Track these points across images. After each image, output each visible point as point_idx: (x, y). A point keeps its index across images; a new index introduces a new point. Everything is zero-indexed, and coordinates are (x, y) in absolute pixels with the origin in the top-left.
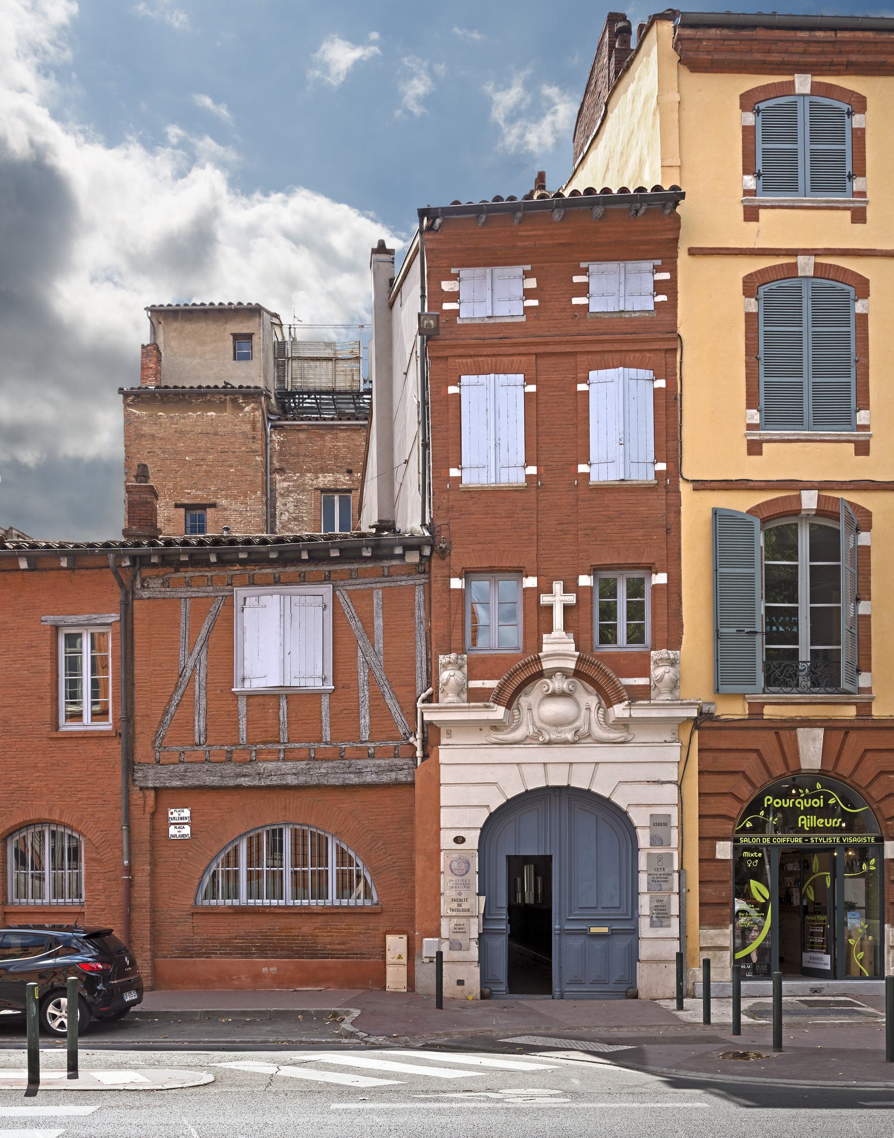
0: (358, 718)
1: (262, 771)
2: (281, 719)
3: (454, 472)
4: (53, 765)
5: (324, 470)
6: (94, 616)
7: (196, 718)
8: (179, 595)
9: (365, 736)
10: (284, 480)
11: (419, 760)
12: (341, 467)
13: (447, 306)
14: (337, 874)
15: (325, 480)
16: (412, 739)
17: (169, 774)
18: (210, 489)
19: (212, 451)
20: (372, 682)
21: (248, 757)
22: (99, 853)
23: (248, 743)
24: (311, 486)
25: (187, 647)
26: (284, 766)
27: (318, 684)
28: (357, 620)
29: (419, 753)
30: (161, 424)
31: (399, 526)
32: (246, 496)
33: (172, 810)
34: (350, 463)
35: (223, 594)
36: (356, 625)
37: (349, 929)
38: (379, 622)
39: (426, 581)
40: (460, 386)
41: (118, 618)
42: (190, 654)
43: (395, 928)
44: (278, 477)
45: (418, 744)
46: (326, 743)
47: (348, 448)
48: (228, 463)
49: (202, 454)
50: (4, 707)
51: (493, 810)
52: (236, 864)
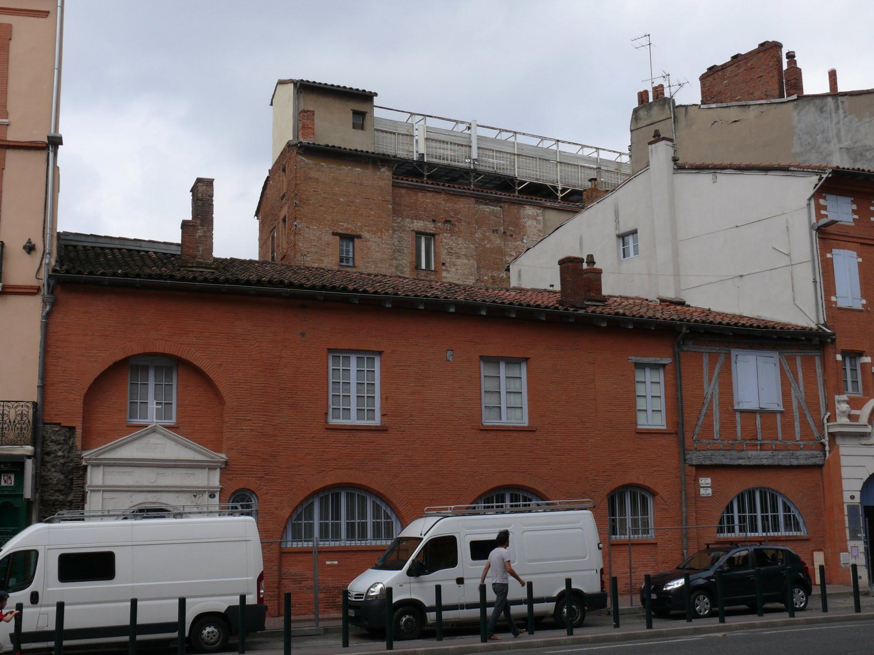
0: (793, 428)
4: (639, 449)
5: (417, 218)
6: (658, 359)
7: (715, 423)
8: (703, 350)
12: (429, 217)
14: (374, 526)
15: (419, 225)
16: (823, 440)
18: (357, 224)
20: (800, 408)
22: (667, 505)
24: (409, 227)
27: (776, 408)
29: (827, 448)
32: (382, 233)
36: (790, 375)
38: (800, 375)
41: (671, 361)
45: (827, 443)
47: (433, 204)
49: (351, 197)
51: (864, 480)
52: (732, 512)
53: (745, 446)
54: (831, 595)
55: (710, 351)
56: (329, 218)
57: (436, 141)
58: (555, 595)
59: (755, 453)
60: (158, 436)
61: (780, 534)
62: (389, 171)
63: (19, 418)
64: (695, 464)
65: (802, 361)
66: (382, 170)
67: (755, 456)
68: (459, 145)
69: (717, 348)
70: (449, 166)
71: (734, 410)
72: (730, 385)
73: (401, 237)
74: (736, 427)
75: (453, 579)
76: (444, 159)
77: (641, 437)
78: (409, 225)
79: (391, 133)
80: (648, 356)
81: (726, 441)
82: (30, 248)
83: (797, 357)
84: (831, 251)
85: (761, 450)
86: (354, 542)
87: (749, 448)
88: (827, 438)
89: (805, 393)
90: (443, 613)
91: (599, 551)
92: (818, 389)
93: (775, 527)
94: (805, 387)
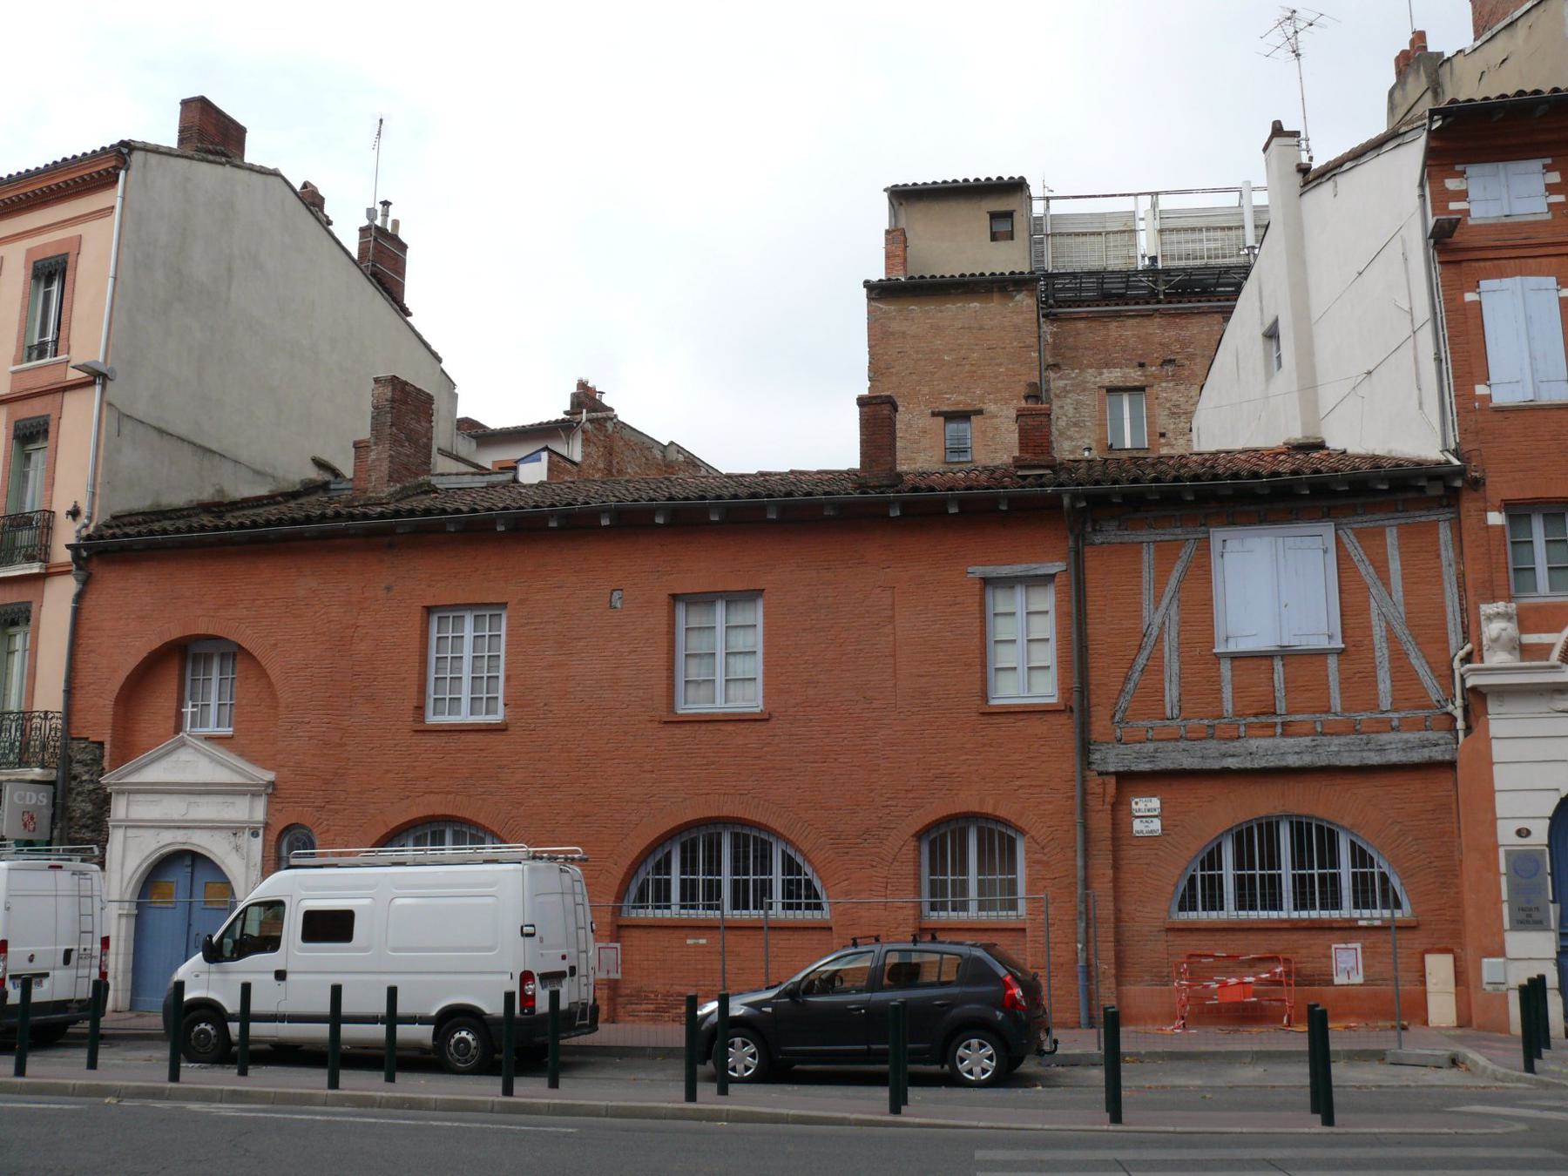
0: (1375, 684)
1: (1255, 749)
2: (1277, 685)
3: (1480, 390)
4: (984, 745)
6: (1034, 566)
8: (1140, 539)
9: (1385, 703)
10: (1060, 378)
11: (1461, 735)
13: (1453, 206)
15: (1112, 376)
16: (1450, 708)
17: (1134, 755)
19: (977, 348)
20: (1392, 638)
21: (1236, 734)
22: (1045, 854)
23: (1235, 715)
24: (1095, 383)
25: (1152, 600)
26: (1283, 744)
27: (1324, 643)
28: (1367, 563)
29: (1460, 724)
30: (913, 319)
31: (1327, 445)
33: (1137, 800)
34: (1141, 356)
35: (1195, 536)
36: (1366, 571)
37: (1375, 947)
38: (1395, 566)
39: (1452, 516)
40: (1479, 293)
41: (1064, 568)
42: (1157, 608)
43: (1436, 946)
44: (1052, 375)
45: (1459, 713)
46: (1335, 714)
47: (1139, 337)
48: (998, 361)
50: (922, 676)
53: (1242, 729)
54: (1139, 1058)
55: (1159, 539)
56: (926, 390)
57: (1178, 230)
58: (433, 1013)
59: (1265, 743)
60: (190, 750)
61: (1223, 915)
62: (1031, 296)
63: (53, 733)
64: (1112, 770)
65: (1400, 537)
66: (1018, 297)
67: (1266, 750)
68: (1223, 229)
69: (1179, 531)
70: (1206, 267)
71: (1215, 654)
72: (1208, 603)
73: (1078, 402)
74: (1220, 691)
75: (271, 972)
76: (1195, 258)
77: (990, 721)
78: (1093, 379)
79: (1093, 234)
80: (1014, 563)
81: (1196, 721)
82: (74, 513)
83: (1388, 530)
84: (1478, 287)
85: (1284, 735)
86: (994, 913)
87: (1254, 732)
88: (1459, 702)
89: (1407, 604)
90: (399, 1027)
91: (521, 939)
92: (1442, 594)
93: (1212, 896)
94: (1407, 592)
